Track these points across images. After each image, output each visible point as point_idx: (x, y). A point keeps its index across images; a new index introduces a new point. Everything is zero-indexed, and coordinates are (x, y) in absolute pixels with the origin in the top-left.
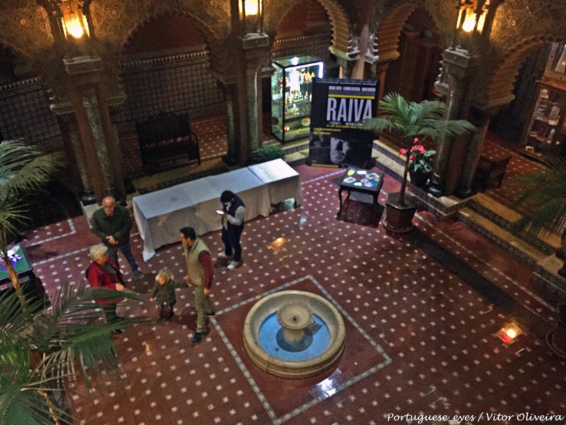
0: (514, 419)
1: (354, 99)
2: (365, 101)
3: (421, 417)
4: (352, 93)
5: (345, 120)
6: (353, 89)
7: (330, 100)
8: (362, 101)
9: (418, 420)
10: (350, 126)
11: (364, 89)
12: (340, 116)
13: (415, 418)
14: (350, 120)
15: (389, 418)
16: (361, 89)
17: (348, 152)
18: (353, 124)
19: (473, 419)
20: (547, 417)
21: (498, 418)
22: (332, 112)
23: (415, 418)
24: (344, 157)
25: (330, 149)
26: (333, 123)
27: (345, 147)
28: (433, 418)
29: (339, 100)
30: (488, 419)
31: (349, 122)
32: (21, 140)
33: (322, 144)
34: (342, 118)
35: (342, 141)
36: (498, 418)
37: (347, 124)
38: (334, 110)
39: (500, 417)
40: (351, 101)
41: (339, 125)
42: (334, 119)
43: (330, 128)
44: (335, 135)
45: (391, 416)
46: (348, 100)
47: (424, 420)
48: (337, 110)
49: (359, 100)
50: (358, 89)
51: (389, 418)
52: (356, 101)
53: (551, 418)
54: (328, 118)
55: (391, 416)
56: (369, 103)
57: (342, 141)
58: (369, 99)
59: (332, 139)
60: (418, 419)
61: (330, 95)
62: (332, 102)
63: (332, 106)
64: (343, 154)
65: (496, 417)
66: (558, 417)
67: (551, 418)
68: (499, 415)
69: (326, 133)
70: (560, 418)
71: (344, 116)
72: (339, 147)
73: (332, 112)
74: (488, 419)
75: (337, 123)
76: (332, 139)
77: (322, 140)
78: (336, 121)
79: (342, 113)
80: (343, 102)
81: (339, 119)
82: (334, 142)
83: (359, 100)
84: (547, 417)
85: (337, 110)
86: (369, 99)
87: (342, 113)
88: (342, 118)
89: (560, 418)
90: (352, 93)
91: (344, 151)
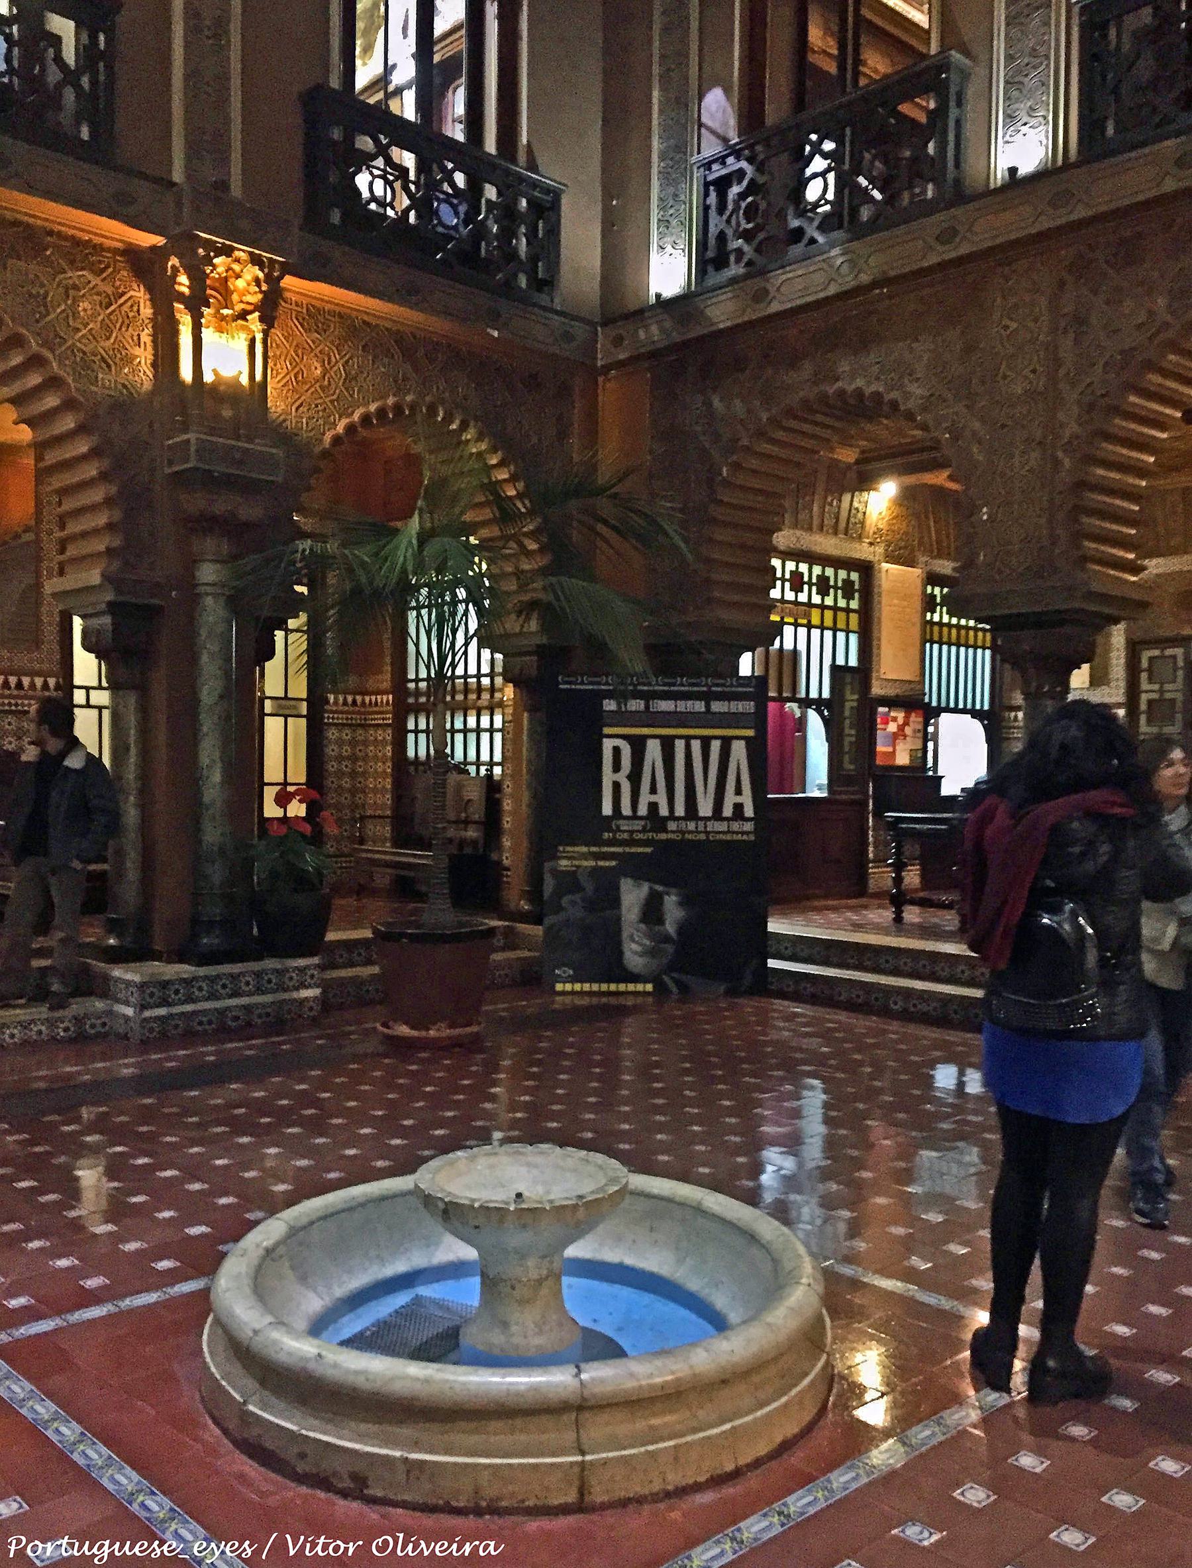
0: (364, 1551)
1: (688, 739)
2: (726, 742)
3: (102, 1546)
4: (681, 719)
5: (664, 811)
6: (682, 706)
7: (608, 745)
8: (716, 745)
9: (94, 1556)
10: (683, 833)
11: (717, 707)
12: (645, 798)
13: (86, 1548)
14: (680, 811)
15: (13, 1548)
16: (708, 706)
17: (682, 929)
18: (691, 826)
19: (249, 1551)
20: (455, 1546)
21: (319, 1548)
22: (617, 786)
23: (86, 1548)
24: (670, 948)
25: (619, 919)
26: (625, 826)
27: (673, 911)
28: (136, 1550)
29: (638, 745)
30: (292, 1553)
31: (678, 819)
32: (923, 1445)
33: (591, 906)
34: (653, 807)
35: (659, 888)
36: (319, 1548)
37: (672, 826)
38: (622, 777)
39: (325, 1547)
40: (680, 745)
41: (644, 830)
42: (626, 811)
43: (610, 843)
44: (637, 868)
45: (19, 1542)
46: (668, 745)
47: (111, 1554)
48: (635, 778)
49: (706, 742)
50: (700, 706)
51: (13, 1548)
52: (696, 745)
53: (467, 1548)
54: (607, 809)
55: (19, 1542)
56: (739, 750)
57: (659, 888)
58: (716, 738)
59: (626, 885)
60: (95, 1550)
61: (606, 731)
62: (617, 751)
63: (617, 767)
64: (667, 939)
65: (314, 1545)
66: (487, 1546)
67: (467, 1548)
68: (322, 1540)
69: (601, 863)
70: (491, 1548)
71: (661, 799)
72: (652, 912)
73: (617, 786)
74: (292, 1553)
75: (638, 825)
76: (626, 885)
77: (589, 887)
78: (635, 817)
79: (653, 791)
80: (653, 749)
81: (643, 810)
82: (632, 896)
83: (706, 742)
84: (455, 1546)
85: (635, 778)
86: (716, 738)
87: (653, 791)
88: (653, 807)
89: (491, 1548)
90: (681, 719)
91: (670, 928)
